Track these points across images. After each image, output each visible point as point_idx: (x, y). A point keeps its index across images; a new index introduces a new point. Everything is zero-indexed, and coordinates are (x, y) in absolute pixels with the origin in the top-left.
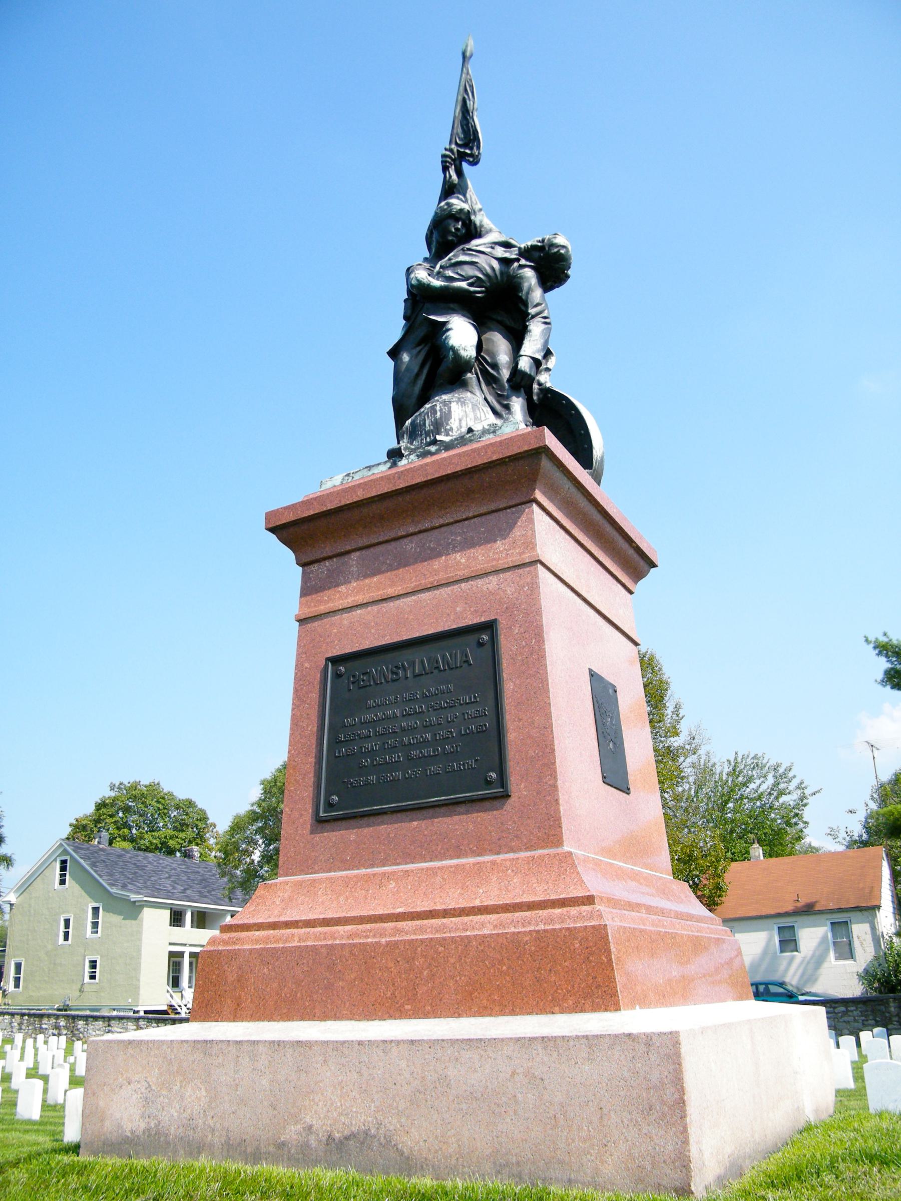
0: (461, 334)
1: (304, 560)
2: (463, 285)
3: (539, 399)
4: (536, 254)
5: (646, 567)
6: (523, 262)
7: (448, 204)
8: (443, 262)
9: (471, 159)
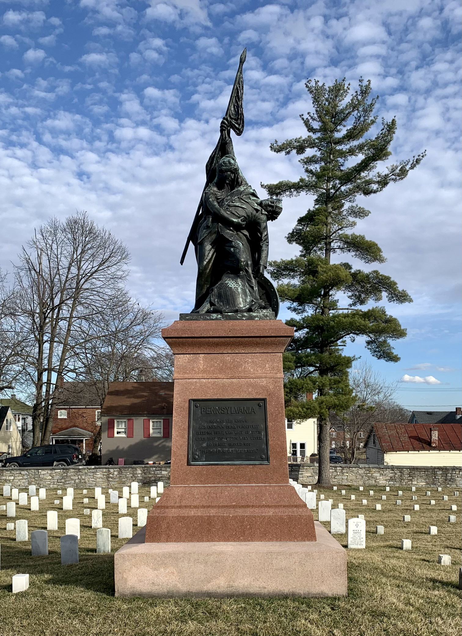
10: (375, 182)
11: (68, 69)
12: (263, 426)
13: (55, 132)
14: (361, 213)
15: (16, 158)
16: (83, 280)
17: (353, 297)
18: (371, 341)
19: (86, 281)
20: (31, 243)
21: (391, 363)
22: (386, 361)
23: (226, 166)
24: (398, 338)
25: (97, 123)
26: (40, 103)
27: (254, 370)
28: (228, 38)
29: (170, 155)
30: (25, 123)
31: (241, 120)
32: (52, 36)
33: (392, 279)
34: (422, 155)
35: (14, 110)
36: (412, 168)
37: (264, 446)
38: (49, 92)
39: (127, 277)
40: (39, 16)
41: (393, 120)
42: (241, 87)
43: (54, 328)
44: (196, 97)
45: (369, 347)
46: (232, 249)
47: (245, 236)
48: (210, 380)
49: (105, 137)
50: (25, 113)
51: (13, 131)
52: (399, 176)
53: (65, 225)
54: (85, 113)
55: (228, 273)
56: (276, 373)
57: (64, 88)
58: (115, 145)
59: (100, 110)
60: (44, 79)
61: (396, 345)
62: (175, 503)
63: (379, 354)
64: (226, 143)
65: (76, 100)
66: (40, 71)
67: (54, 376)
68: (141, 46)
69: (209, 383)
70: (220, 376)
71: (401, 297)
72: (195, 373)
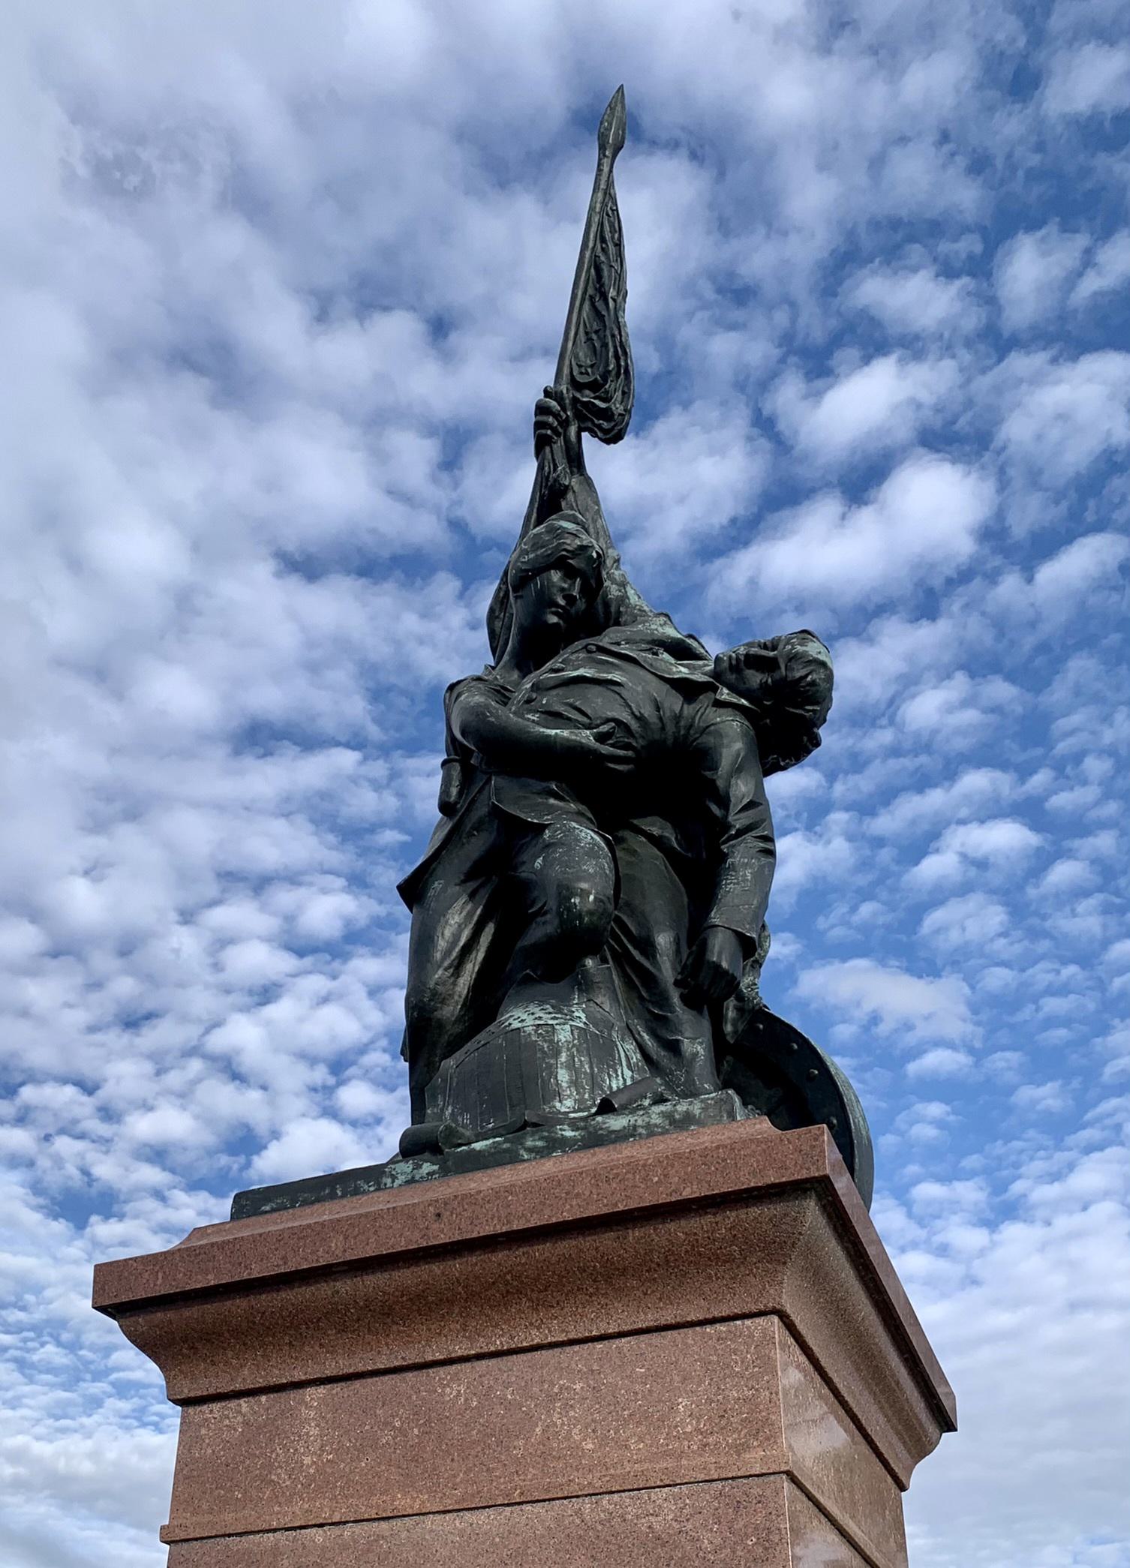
0: (579, 860)
1: (186, 1393)
2: (586, 737)
3: (735, 1032)
4: (755, 678)
5: (931, 1428)
6: (725, 694)
7: (552, 530)
8: (544, 674)
9: (605, 425)
28: (1080, 1079)
29: (976, 1292)
44: (1018, 1187)
47: (657, 841)
48: (348, 1531)
56: (741, 1448)
68: (901, 1120)
69: (345, 1547)
70: (402, 1502)
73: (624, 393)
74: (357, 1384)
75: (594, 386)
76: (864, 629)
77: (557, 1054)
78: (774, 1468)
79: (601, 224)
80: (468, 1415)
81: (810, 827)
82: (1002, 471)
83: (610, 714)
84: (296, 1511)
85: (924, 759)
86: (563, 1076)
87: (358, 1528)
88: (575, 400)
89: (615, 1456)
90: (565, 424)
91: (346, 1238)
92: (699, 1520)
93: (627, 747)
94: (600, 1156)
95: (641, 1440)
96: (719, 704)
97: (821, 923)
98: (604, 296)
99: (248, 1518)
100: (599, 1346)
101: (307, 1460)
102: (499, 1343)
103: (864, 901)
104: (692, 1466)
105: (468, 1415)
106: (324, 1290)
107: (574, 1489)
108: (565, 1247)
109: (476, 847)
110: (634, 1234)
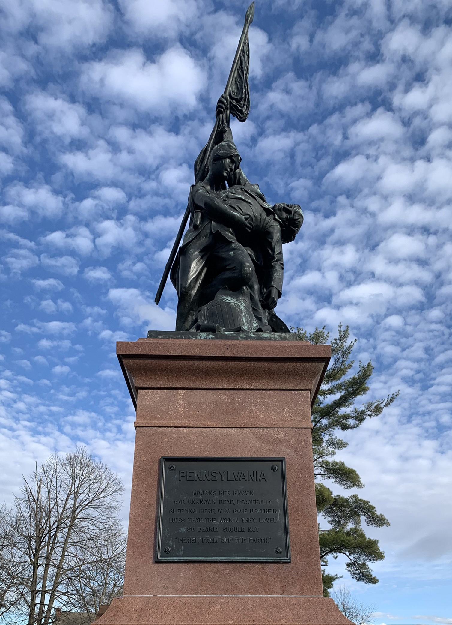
4: (285, 215)
9: (241, 115)
10: (352, 418)
11: (87, 380)
12: (279, 501)
13: (74, 425)
14: (341, 445)
15: (41, 443)
16: (78, 510)
17: (332, 523)
18: (351, 564)
19: (81, 510)
20: (33, 477)
21: (370, 585)
22: (365, 583)
23: (223, 149)
24: (376, 560)
25: (108, 419)
26: (64, 404)
27: (265, 416)
30: (51, 419)
31: (245, 100)
32: (77, 358)
33: (370, 504)
34: (396, 394)
35: (42, 408)
36: (386, 405)
37: (281, 534)
38: (72, 396)
39: (121, 508)
40: (67, 344)
41: (369, 363)
42: (246, 57)
43: (49, 554)
45: (349, 569)
46: (231, 253)
48: (194, 429)
49: (115, 430)
50: (50, 411)
51: (39, 423)
52: (374, 412)
53: (65, 460)
54: (100, 412)
55: (225, 288)
56: (300, 421)
57: (82, 394)
58: (123, 435)
59: (111, 411)
60: (68, 387)
61: (374, 567)
62: (130, 620)
63: (358, 576)
64: (225, 132)
65: (92, 403)
66: (65, 380)
67: (47, 597)
69: (193, 434)
70: (210, 423)
71: (379, 521)
72: (170, 419)
73: (247, 107)
74: (195, 391)
75: (237, 100)
76: (149, 127)
77: (242, 313)
78: (309, 427)
79: (244, 46)
80: (228, 404)
81: (118, 219)
82: (210, 68)
83: (249, 213)
84: (178, 422)
85: (167, 201)
86: (244, 319)
87: (197, 429)
88: (231, 102)
89: (268, 419)
90: (227, 109)
91: (200, 350)
92: (290, 437)
93: (251, 224)
94: (258, 343)
95: (275, 416)
96: (275, 219)
97: (121, 266)
98: (242, 71)
99: (162, 422)
100: (264, 392)
101: (180, 410)
102: (238, 387)
103: (138, 262)
104: (288, 424)
105: (228, 404)
106: (191, 363)
107: (258, 426)
108: (260, 364)
109: (204, 241)
110: (279, 364)
